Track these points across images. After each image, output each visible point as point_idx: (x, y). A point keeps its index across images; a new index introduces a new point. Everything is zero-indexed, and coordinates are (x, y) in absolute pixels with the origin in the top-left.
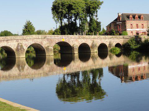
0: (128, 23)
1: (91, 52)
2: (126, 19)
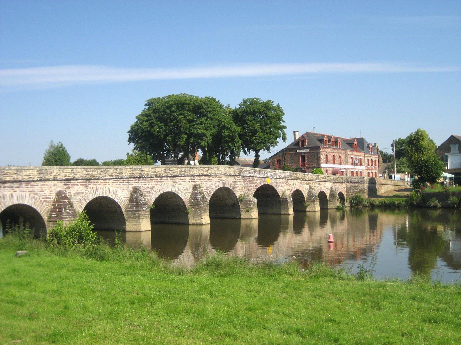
0: (326, 152)
1: (305, 211)
2: (319, 144)
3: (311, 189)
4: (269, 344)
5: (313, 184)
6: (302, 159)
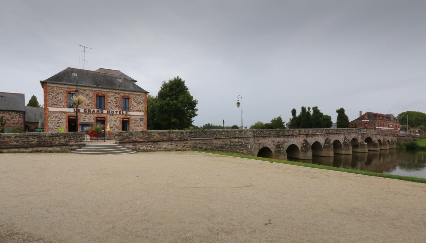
3: (345, 138)
4: (210, 242)
5: (386, 137)
6: (127, 106)
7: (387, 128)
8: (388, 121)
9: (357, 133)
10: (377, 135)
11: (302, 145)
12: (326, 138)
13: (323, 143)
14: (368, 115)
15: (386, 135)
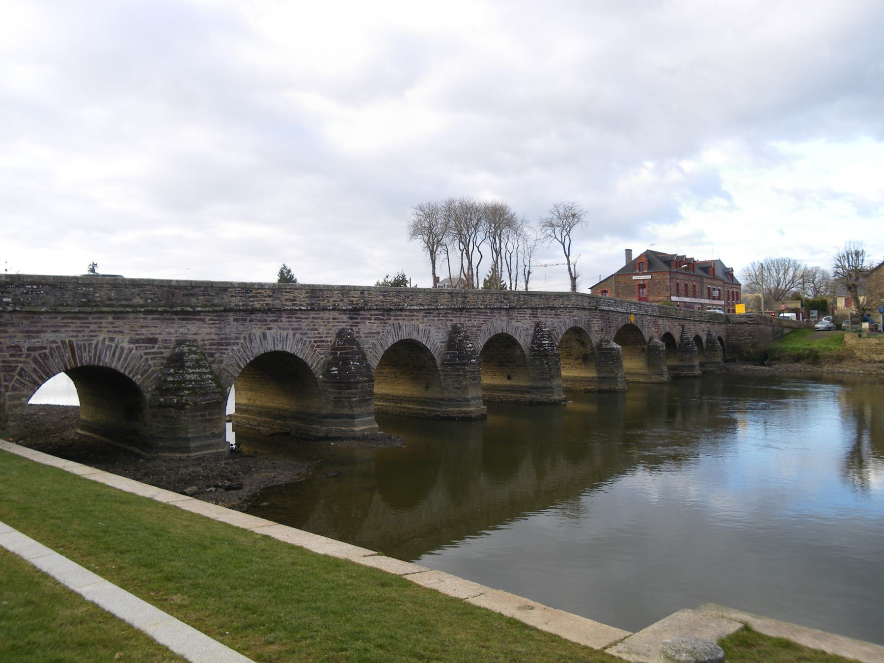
5: (689, 326)
7: (706, 301)
8: (706, 281)
9: (584, 309)
10: (659, 317)
11: (331, 354)
12: (454, 327)
13: (439, 345)
14: (649, 261)
15: (690, 317)
